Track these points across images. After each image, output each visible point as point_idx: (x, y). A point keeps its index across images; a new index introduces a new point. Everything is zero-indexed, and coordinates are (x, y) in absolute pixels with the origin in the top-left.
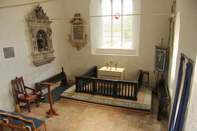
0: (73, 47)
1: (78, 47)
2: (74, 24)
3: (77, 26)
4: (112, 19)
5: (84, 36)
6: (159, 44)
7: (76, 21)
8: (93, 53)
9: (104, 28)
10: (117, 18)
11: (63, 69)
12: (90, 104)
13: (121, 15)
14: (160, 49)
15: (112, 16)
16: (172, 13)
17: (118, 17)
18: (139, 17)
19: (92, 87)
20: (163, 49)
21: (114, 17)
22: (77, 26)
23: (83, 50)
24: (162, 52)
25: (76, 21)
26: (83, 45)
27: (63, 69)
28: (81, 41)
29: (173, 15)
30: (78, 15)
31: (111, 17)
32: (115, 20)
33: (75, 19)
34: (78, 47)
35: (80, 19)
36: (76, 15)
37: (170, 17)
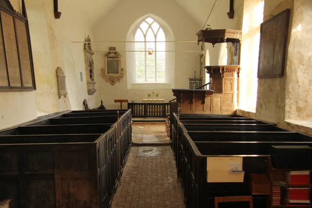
0: (106, 81)
1: (112, 82)
2: (108, 58)
3: (111, 59)
4: (146, 54)
5: (119, 71)
6: (192, 77)
7: (111, 55)
8: (129, 87)
9: (137, 63)
10: (150, 54)
11: (102, 103)
12: (145, 123)
13: (144, 50)
14: (194, 80)
15: (145, 51)
16: (202, 50)
17: (152, 53)
18: (128, 38)
19: (98, 181)
20: (196, 80)
21: (147, 53)
22: (111, 59)
23: (117, 84)
24: (196, 83)
25: (111, 55)
26: (119, 79)
27: (102, 103)
28: (116, 75)
29: (204, 52)
30: (112, 48)
31: (144, 53)
32: (148, 56)
33: (109, 53)
34: (112, 82)
35: (116, 53)
36: (111, 49)
37: (201, 53)
